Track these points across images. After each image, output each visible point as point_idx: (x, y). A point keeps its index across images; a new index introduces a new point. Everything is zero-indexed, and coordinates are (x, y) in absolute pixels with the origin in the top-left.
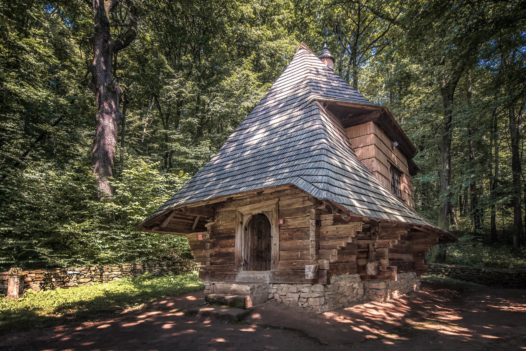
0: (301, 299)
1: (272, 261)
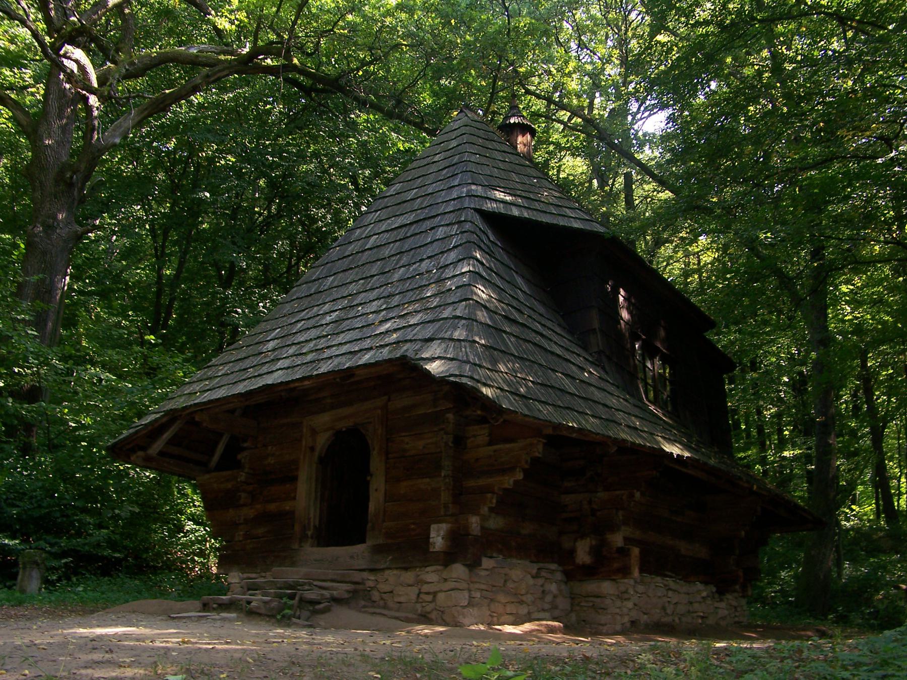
0: (422, 596)
1: (369, 525)
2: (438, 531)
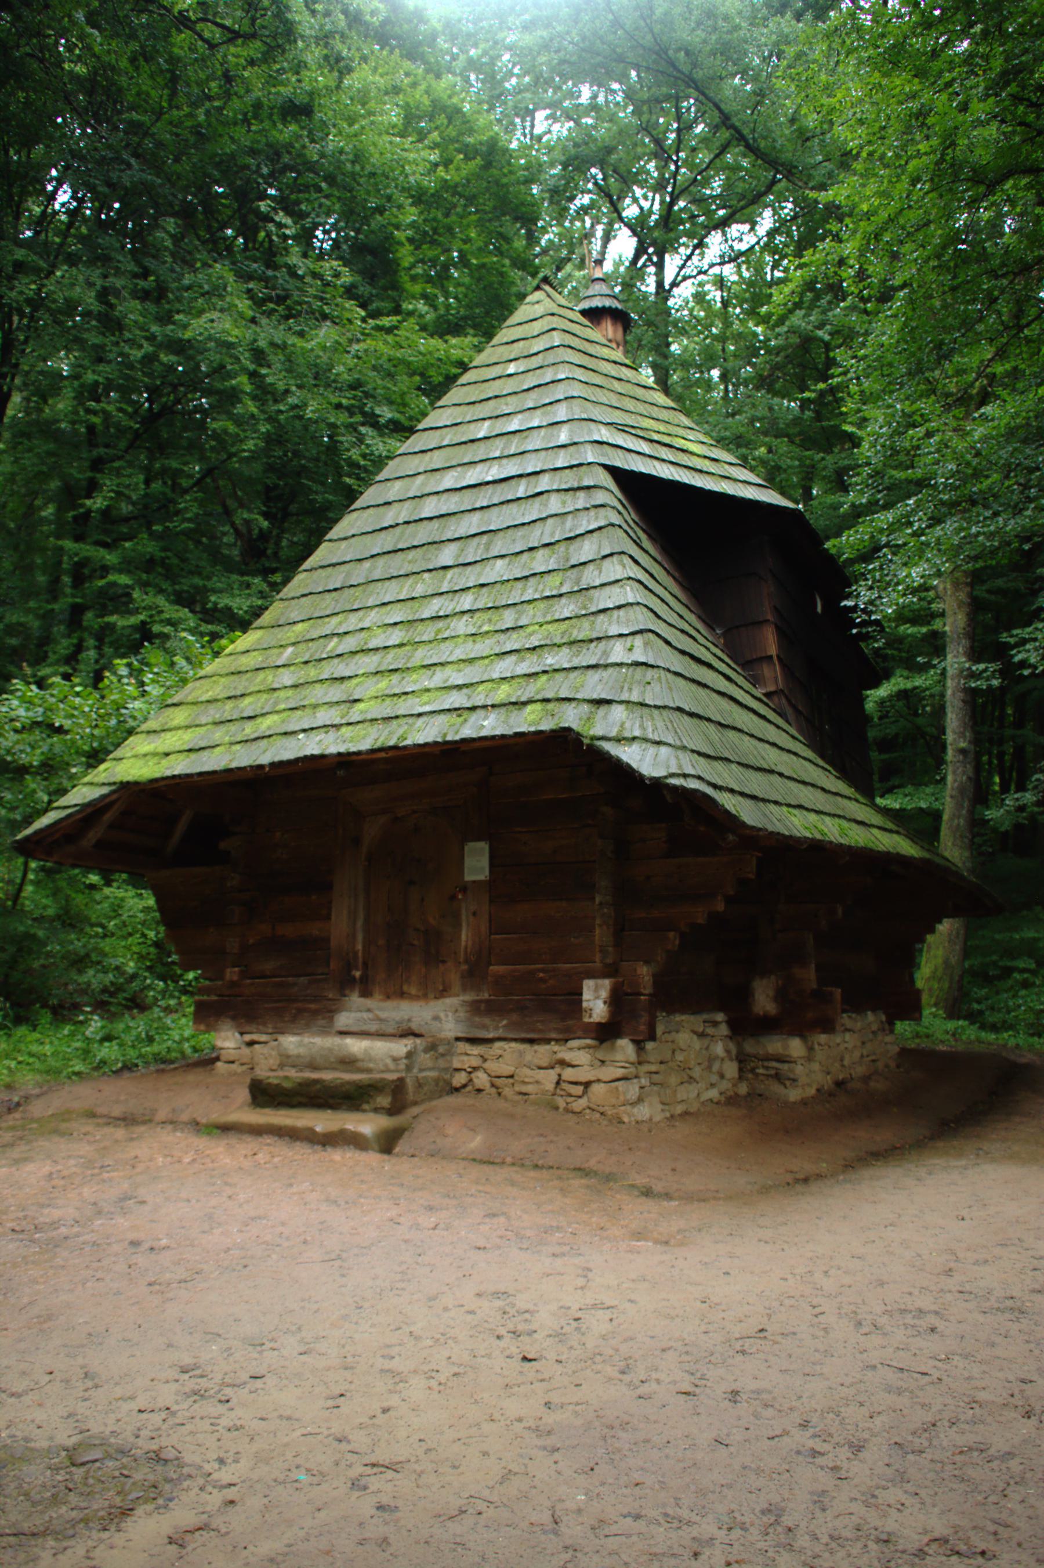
0: (564, 1085)
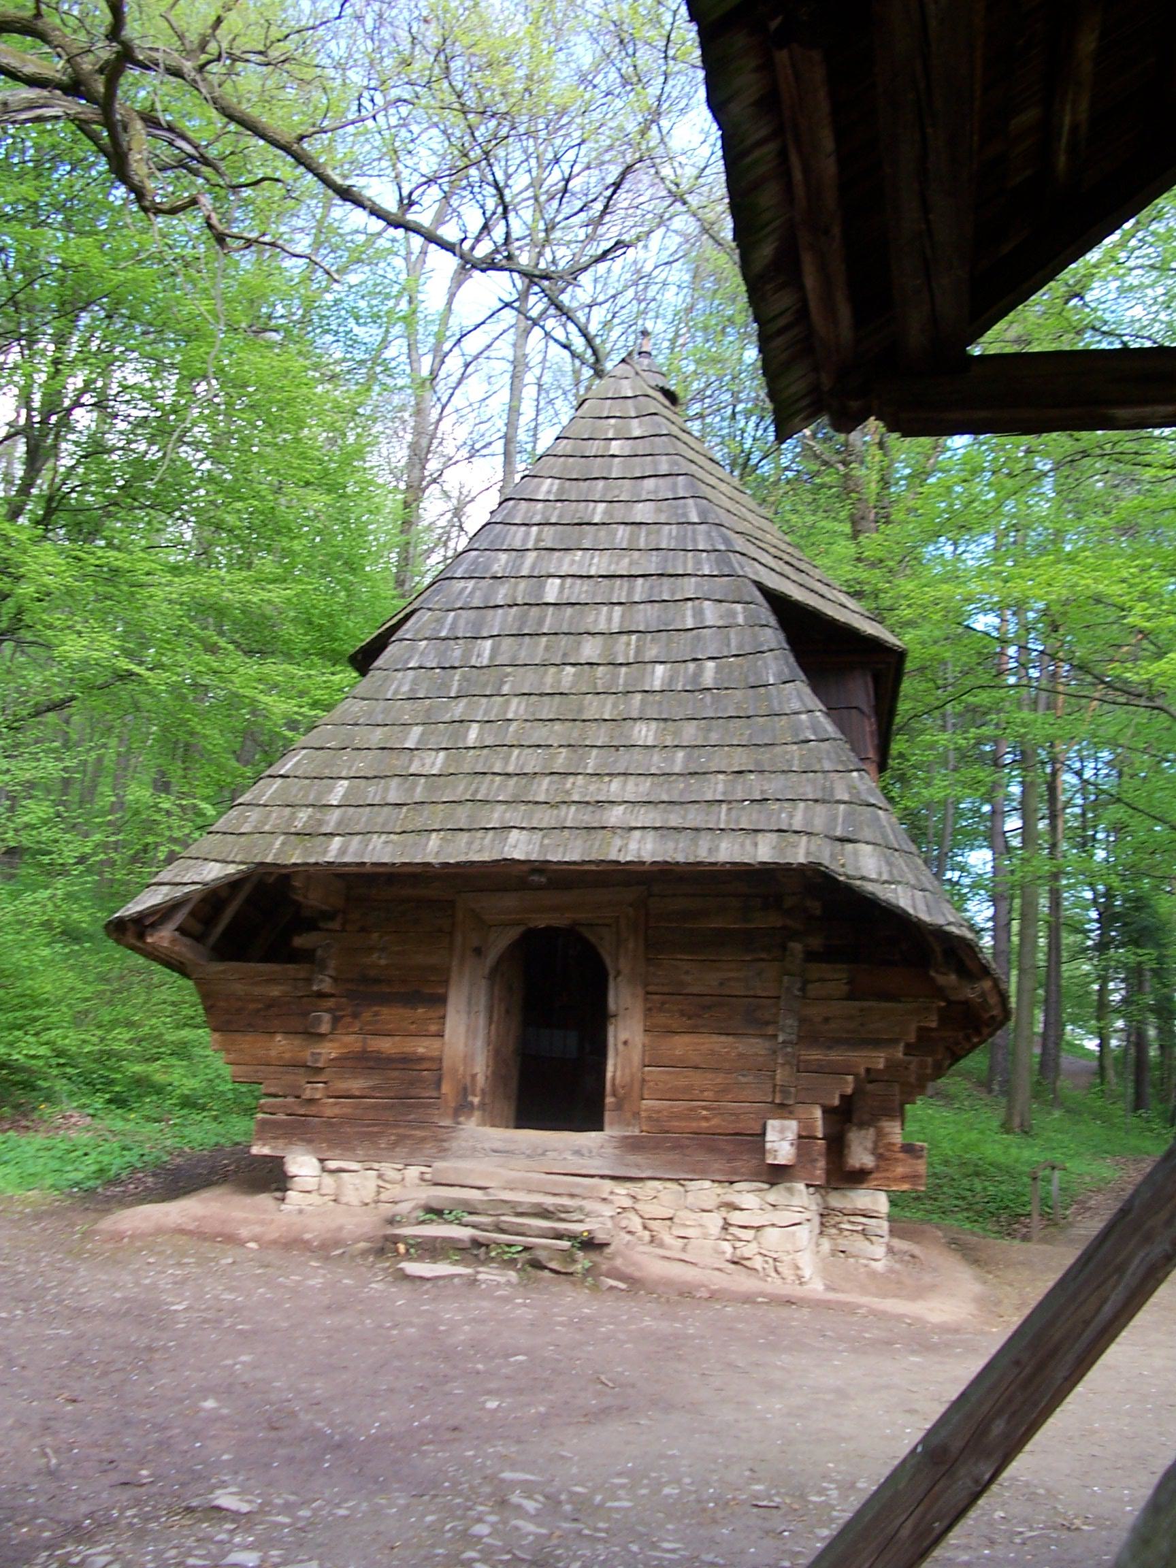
2: (782, 1131)
